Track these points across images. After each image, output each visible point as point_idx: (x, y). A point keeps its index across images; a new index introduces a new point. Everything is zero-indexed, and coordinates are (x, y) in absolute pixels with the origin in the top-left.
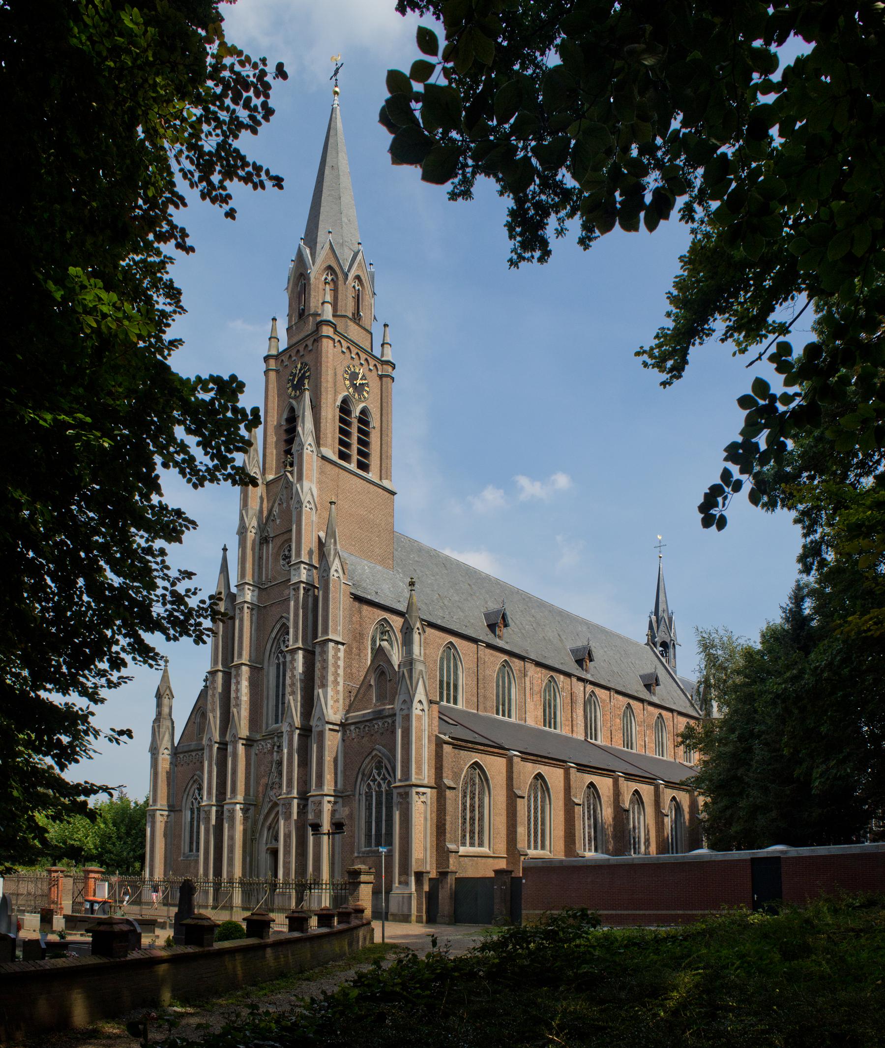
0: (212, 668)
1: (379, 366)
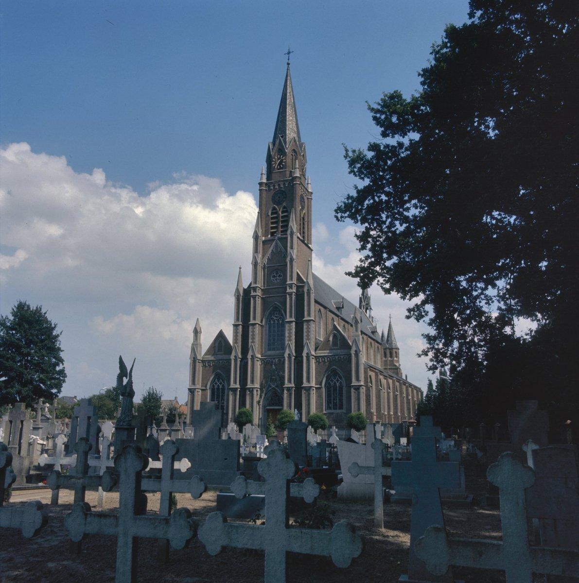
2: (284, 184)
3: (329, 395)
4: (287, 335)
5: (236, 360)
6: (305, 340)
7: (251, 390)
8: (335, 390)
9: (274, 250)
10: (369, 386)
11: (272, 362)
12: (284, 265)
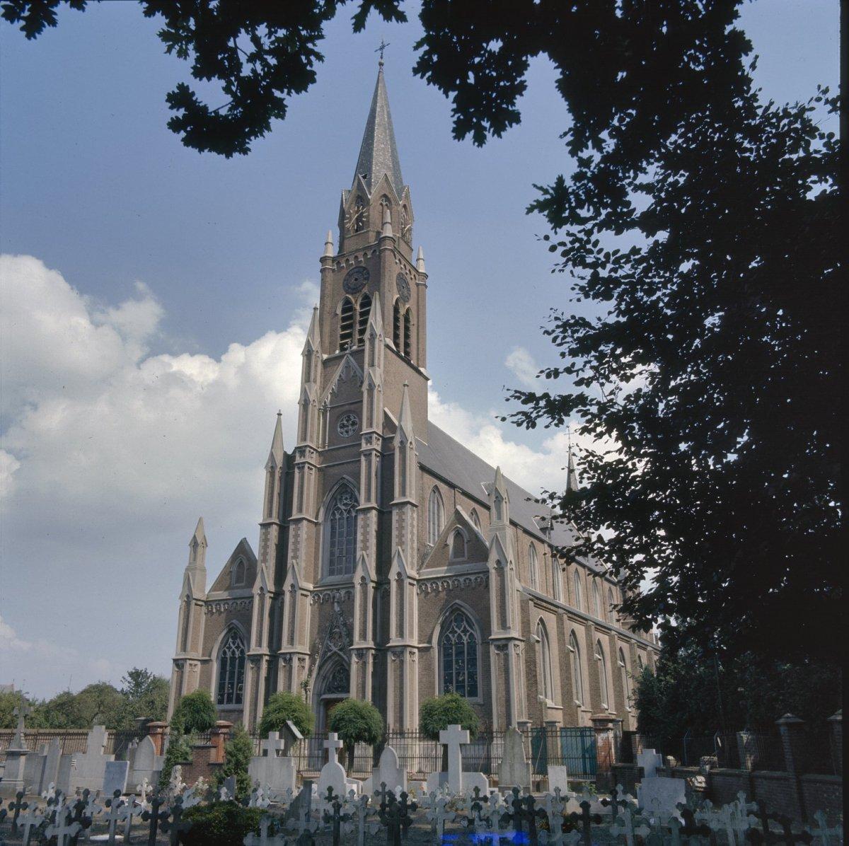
0: (263, 520)
1: (417, 276)
2: (365, 254)
3: (447, 666)
4: (359, 537)
5: (262, 596)
6: (394, 544)
7: (288, 659)
8: (460, 653)
9: (343, 376)
10: (532, 641)
11: (334, 597)
12: (359, 402)
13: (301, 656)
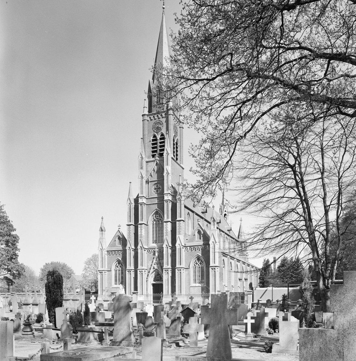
13: (141, 270)
